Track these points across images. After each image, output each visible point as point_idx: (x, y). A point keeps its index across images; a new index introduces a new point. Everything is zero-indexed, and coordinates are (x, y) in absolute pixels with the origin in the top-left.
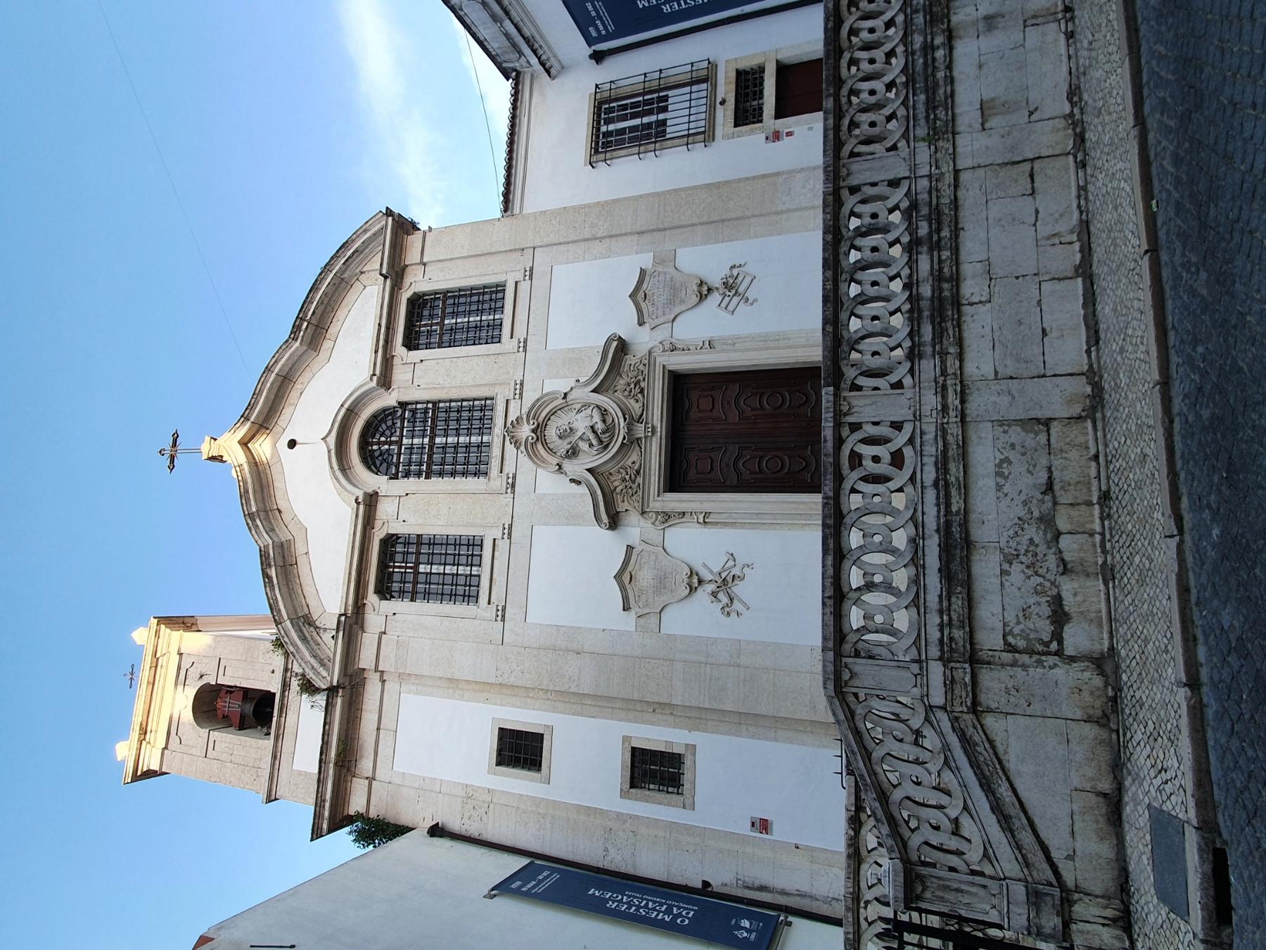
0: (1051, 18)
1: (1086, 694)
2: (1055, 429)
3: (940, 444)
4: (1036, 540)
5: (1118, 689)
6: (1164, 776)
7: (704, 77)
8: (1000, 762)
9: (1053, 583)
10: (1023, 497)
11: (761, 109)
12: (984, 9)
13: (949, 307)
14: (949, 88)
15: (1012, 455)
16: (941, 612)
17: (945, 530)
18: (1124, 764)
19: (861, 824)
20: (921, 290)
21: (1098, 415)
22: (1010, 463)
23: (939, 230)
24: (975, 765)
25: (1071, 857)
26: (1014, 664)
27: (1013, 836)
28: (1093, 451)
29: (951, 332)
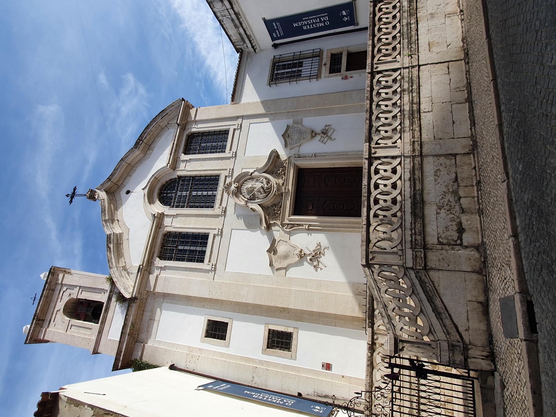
1: (472, 261)
2: (458, 157)
4: (451, 200)
5: (486, 258)
6: (506, 282)
7: (318, 55)
8: (436, 290)
9: (458, 217)
10: (445, 184)
12: (429, 12)
13: (416, 113)
15: (441, 168)
16: (411, 229)
18: (489, 289)
19: (374, 351)
21: (475, 152)
22: (440, 171)
24: (425, 291)
25: (467, 330)
26: (442, 249)
27: (442, 321)
28: (473, 166)
29: (416, 122)
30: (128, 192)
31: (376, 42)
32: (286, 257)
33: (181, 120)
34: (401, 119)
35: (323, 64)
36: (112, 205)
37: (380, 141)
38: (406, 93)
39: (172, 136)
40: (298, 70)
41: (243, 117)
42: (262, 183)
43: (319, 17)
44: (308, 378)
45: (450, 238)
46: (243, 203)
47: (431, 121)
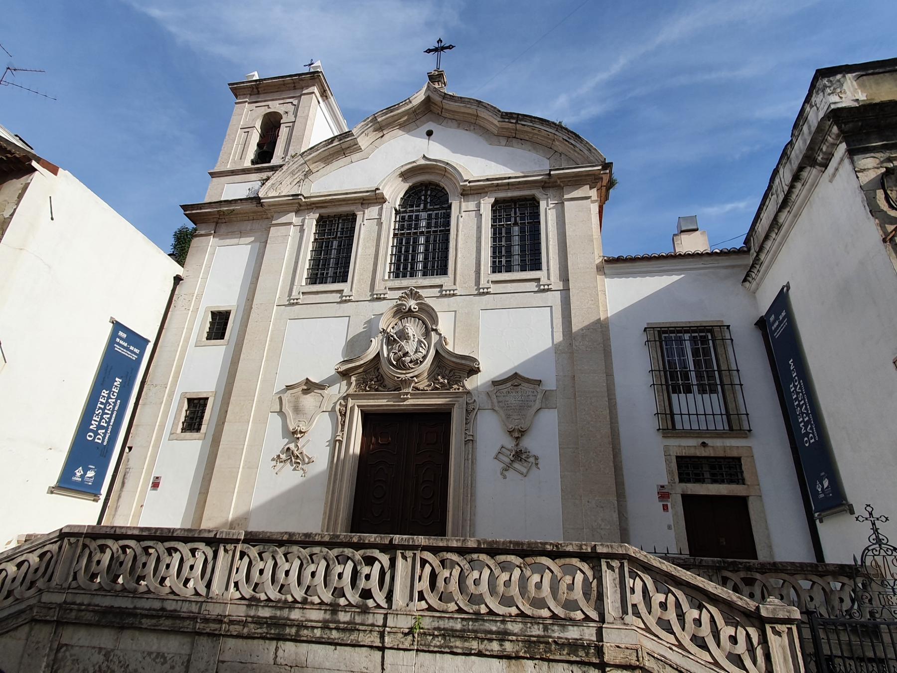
7: (736, 424)
8: (7, 632)
14: (459, 651)
15: (167, 666)
17: (131, 613)
20: (297, 610)
22: (162, 664)
23: (337, 629)
29: (259, 631)
30: (429, 133)
31: (502, 558)
32: (297, 409)
34: (279, 601)
35: (706, 440)
37: (246, 560)
38: (328, 616)
39: (536, 168)
41: (566, 290)
42: (416, 352)
43: (106, 429)
45: (62, 664)
46: (382, 325)
47: (255, 659)
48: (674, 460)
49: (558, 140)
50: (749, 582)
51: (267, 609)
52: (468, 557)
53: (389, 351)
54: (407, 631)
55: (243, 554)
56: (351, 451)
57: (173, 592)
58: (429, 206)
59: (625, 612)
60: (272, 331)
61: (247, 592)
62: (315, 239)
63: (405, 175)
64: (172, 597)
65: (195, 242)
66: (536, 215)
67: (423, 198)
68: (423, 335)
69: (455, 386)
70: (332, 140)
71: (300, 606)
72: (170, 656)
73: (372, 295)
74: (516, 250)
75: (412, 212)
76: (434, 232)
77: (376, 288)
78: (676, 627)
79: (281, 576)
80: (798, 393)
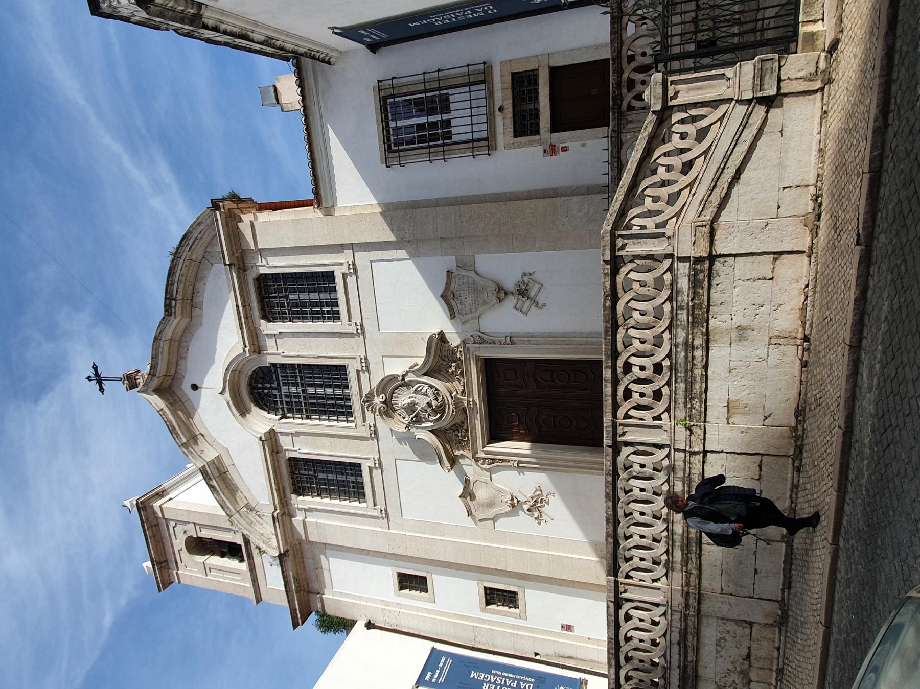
0: (792, 341)
3: (683, 624)
4: (737, 681)
7: (481, 76)
10: (731, 659)
11: (537, 110)
12: (738, 320)
14: (704, 385)
17: (684, 670)
21: (783, 628)
28: (777, 645)
29: (694, 560)
30: (195, 387)
31: (620, 370)
32: (490, 504)
33: (231, 255)
35: (497, 108)
36: (180, 413)
37: (632, 573)
40: (442, 121)
41: (352, 247)
42: (427, 395)
43: (519, 680)
44: (545, 640)
46: (402, 429)
47: (719, 563)
48: (519, 139)
49: (191, 255)
50: (631, 84)
51: (675, 554)
52: (620, 376)
53: (427, 421)
54: (688, 432)
55: (628, 576)
56: (528, 452)
57: (664, 635)
58: (275, 385)
59: (663, 235)
60: (415, 532)
61: (660, 571)
62: (318, 495)
63: (243, 411)
64: (668, 636)
65: (330, 611)
66: (275, 277)
67: (266, 391)
68: (409, 389)
69: (458, 355)
70: (211, 487)
71: (670, 525)
72: (719, 635)
73: (372, 439)
74: (314, 296)
75: (282, 402)
76: (301, 380)
77: (364, 435)
78: (674, 188)
79: (644, 542)
80: (444, 19)
